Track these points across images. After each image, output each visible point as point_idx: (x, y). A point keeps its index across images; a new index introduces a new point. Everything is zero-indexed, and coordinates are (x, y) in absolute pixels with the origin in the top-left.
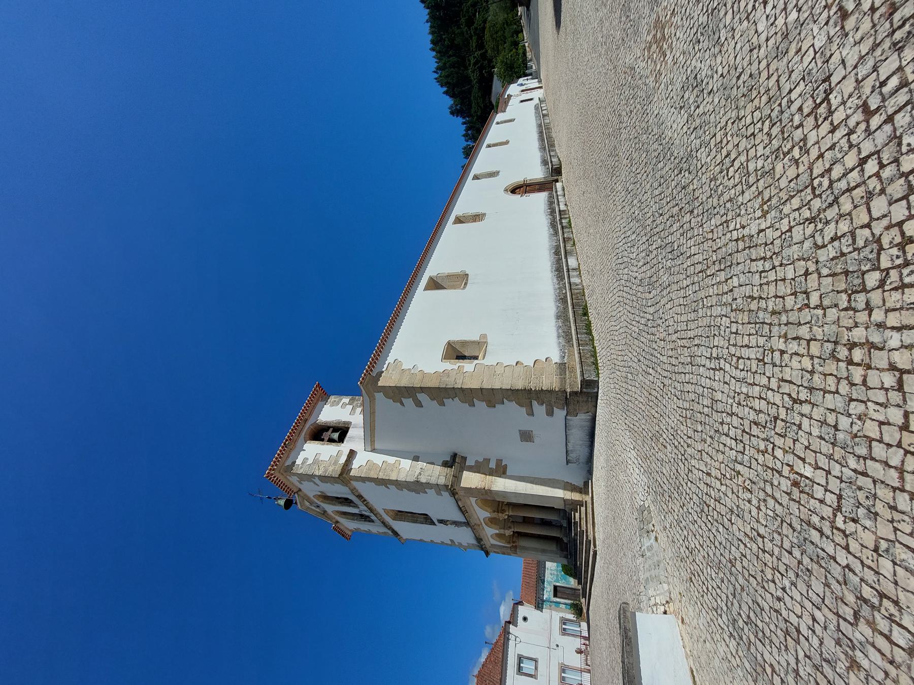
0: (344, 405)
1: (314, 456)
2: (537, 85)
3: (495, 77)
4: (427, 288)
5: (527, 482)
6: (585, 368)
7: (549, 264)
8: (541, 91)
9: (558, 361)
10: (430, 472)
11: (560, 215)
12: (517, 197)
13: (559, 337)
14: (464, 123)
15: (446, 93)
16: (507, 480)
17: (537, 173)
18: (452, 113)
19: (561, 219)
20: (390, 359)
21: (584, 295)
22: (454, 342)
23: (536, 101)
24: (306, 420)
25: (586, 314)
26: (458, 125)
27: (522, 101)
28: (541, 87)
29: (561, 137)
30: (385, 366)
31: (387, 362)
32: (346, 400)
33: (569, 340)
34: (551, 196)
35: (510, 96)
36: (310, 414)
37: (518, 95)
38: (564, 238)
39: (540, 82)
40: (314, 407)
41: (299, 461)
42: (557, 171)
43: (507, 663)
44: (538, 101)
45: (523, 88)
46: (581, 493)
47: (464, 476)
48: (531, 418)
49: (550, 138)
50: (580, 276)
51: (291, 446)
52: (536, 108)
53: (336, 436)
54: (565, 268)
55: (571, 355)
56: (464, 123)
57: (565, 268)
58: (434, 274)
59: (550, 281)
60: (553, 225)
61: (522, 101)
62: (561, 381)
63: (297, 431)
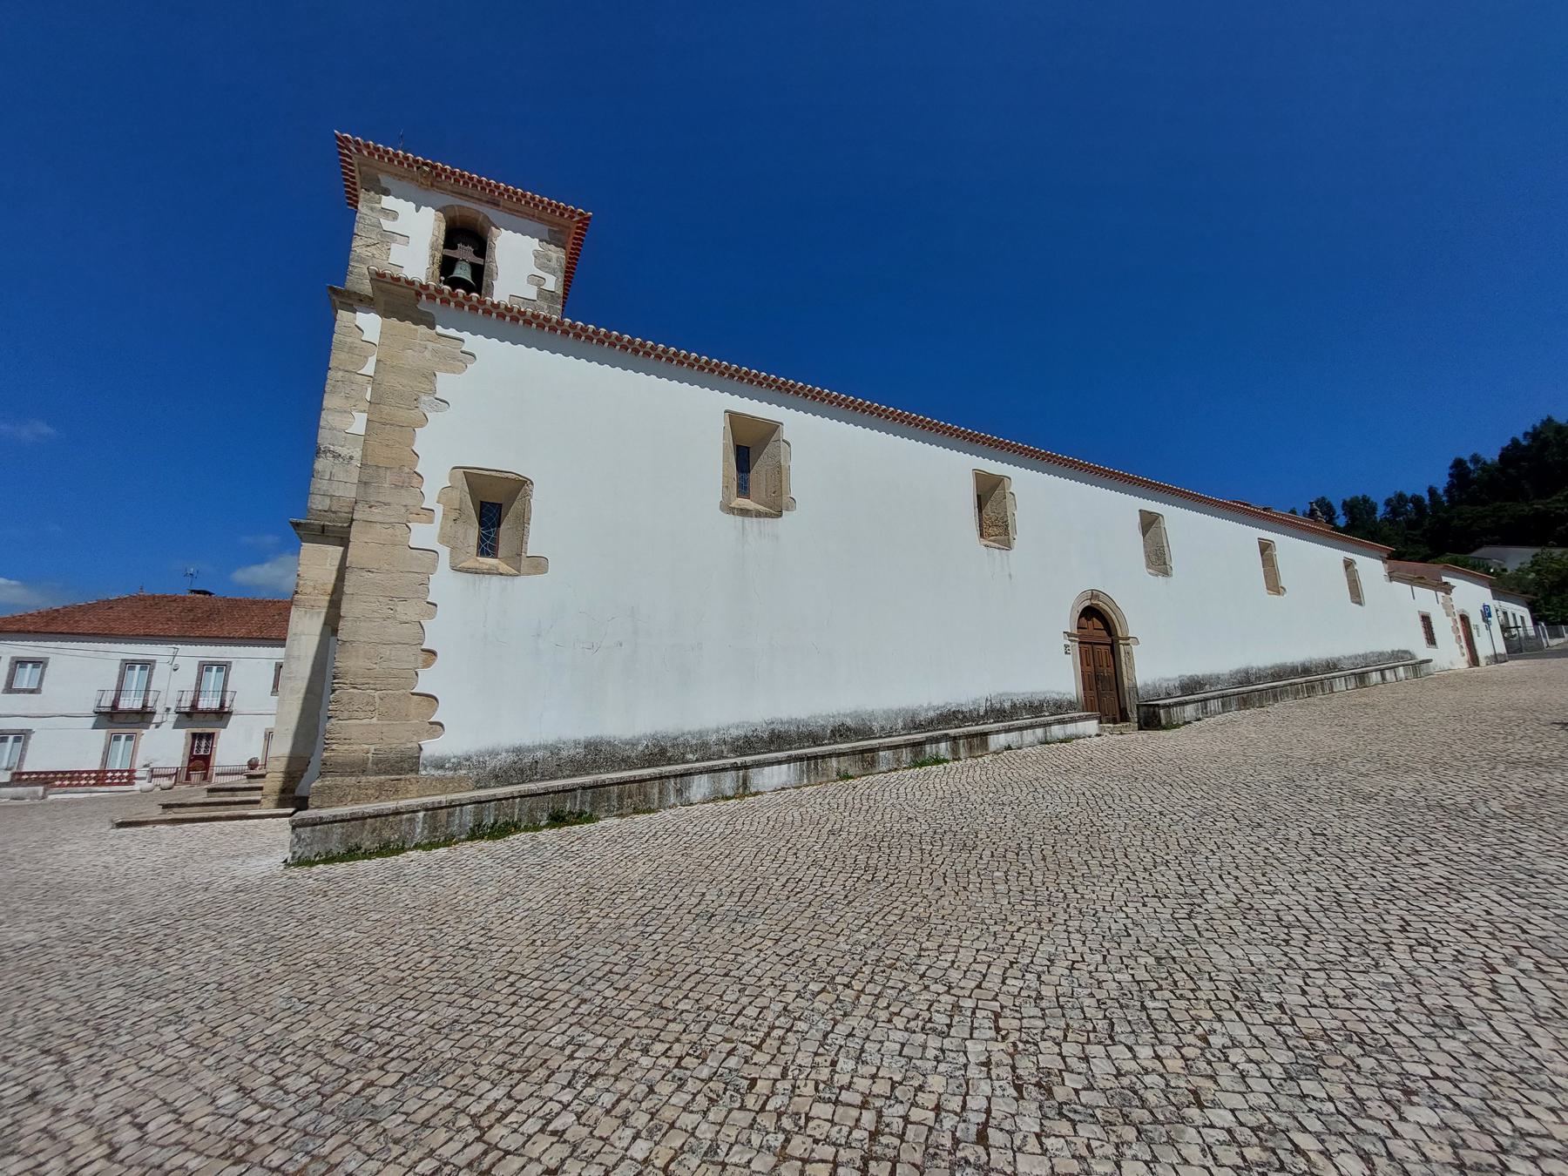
0: (537, 281)
1: (404, 234)
2: (1484, 649)
3: (1537, 550)
4: (734, 419)
5: (311, 681)
6: (338, 829)
7: (785, 716)
8: (1461, 663)
9: (426, 753)
10: (341, 475)
11: (969, 736)
12: (1066, 620)
13: (518, 751)
14: (1432, 492)
15: (1515, 441)
16: (315, 640)
17: (1150, 668)
18: (1459, 464)
19: (955, 739)
20: (473, 342)
21: (636, 811)
22: (528, 495)
23: (1422, 651)
24: (495, 204)
25: (557, 820)
26: (1426, 476)
27: (1426, 619)
28: (1474, 660)
29: (952, 779)
30: (452, 332)
31: (465, 335)
32: (552, 283)
33: (500, 777)
34: (1071, 706)
35: (1448, 589)
36: (511, 211)
37: (1448, 609)
38: (873, 750)
39: (1496, 659)
40: (532, 217)
41: (388, 202)
42: (1151, 719)
43: (211, 644)
44: (1421, 657)
45: (1476, 619)
46: (283, 791)
47: (331, 548)
48: (1425, 610)
49: (1276, 695)
50: (718, 797)
51: (425, 182)
52: (1400, 656)
53: (463, 272)
54: (748, 759)
55: (444, 785)
56: (1432, 492)
57: (748, 759)
58: (786, 433)
59: (736, 720)
60: (950, 717)
61: (1426, 619)
62: (352, 764)
63: (461, 187)
